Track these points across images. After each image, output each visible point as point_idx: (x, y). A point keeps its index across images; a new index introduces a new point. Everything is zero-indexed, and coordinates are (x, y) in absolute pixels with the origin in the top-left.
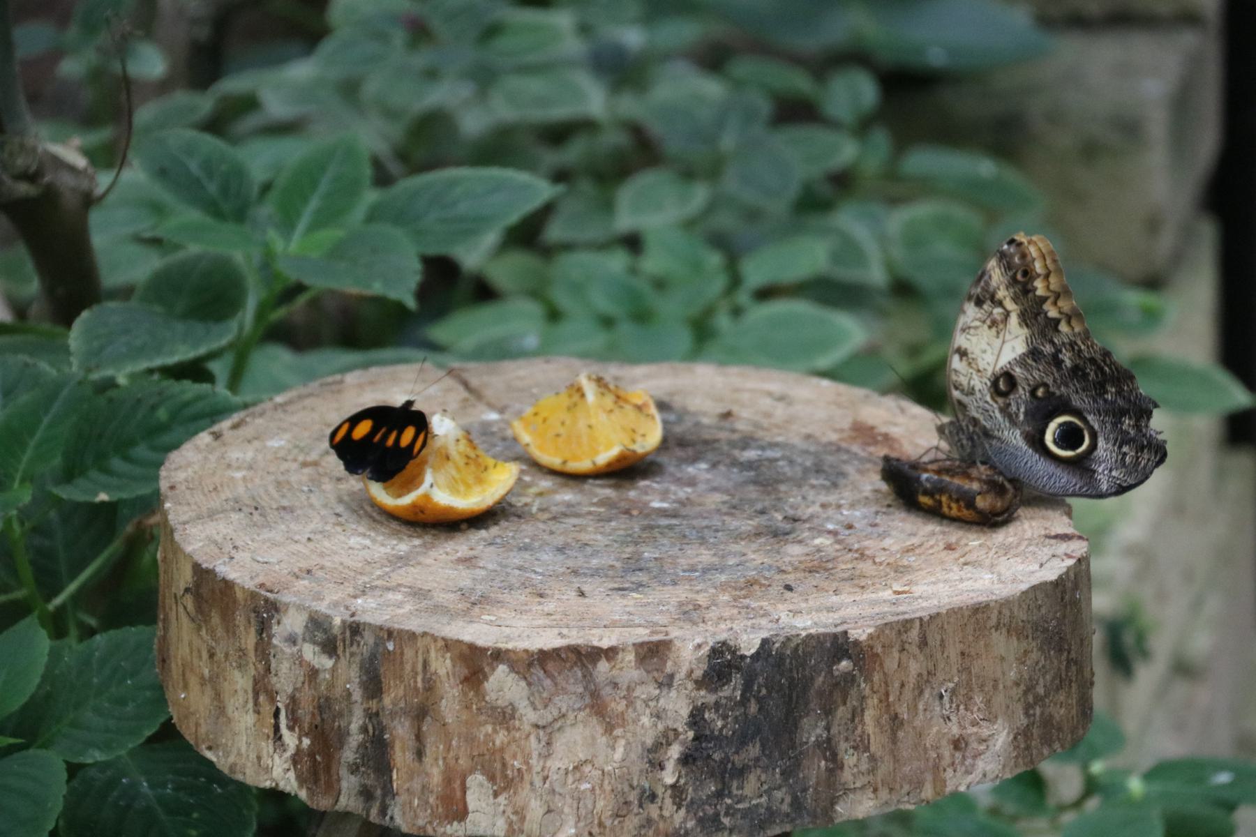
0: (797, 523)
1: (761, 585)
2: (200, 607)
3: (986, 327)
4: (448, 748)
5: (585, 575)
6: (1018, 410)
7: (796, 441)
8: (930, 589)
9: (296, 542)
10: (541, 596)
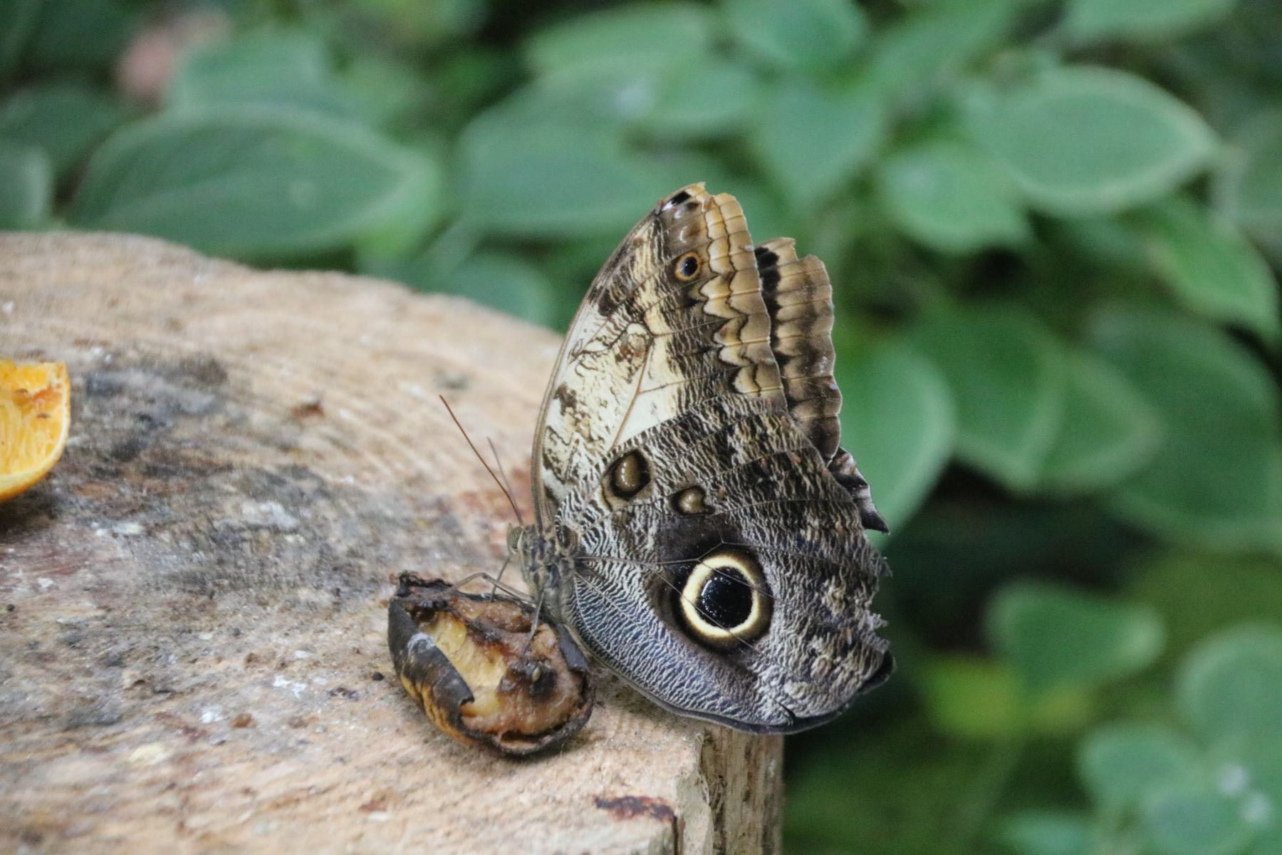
6: (646, 528)
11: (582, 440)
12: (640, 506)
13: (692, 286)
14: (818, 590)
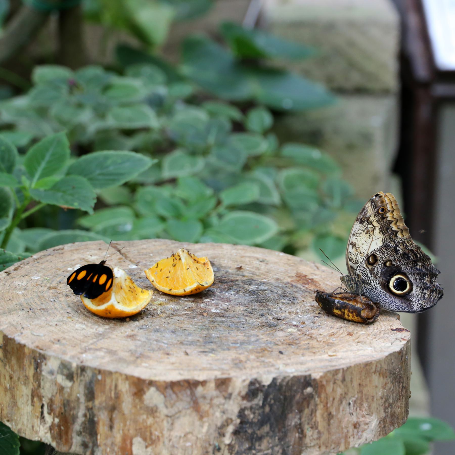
0: (279, 321)
1: (268, 351)
2: (6, 356)
3: (364, 233)
4: (125, 425)
5: (187, 344)
6: (378, 272)
7: (273, 281)
8: (345, 355)
9: (51, 326)
10: (168, 354)
11: (358, 254)
12: (376, 267)
13: (384, 214)
14: (423, 279)
